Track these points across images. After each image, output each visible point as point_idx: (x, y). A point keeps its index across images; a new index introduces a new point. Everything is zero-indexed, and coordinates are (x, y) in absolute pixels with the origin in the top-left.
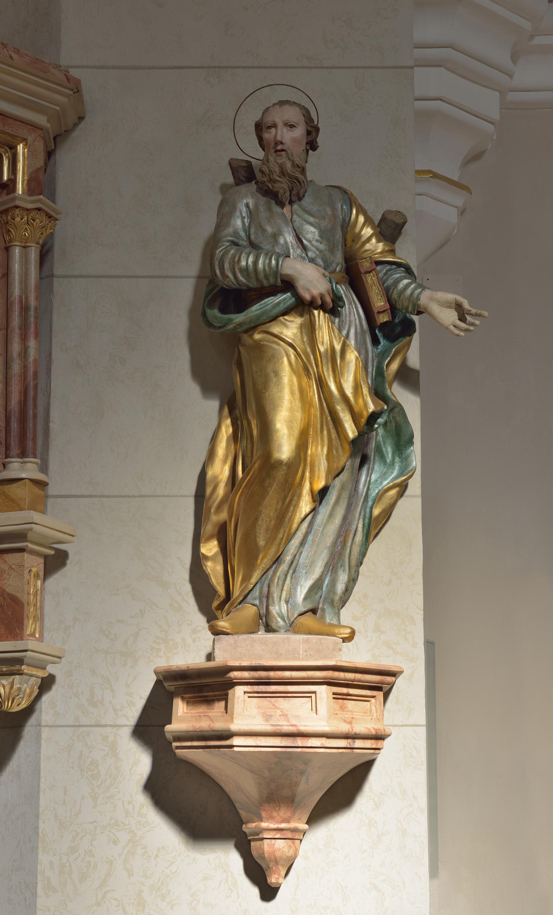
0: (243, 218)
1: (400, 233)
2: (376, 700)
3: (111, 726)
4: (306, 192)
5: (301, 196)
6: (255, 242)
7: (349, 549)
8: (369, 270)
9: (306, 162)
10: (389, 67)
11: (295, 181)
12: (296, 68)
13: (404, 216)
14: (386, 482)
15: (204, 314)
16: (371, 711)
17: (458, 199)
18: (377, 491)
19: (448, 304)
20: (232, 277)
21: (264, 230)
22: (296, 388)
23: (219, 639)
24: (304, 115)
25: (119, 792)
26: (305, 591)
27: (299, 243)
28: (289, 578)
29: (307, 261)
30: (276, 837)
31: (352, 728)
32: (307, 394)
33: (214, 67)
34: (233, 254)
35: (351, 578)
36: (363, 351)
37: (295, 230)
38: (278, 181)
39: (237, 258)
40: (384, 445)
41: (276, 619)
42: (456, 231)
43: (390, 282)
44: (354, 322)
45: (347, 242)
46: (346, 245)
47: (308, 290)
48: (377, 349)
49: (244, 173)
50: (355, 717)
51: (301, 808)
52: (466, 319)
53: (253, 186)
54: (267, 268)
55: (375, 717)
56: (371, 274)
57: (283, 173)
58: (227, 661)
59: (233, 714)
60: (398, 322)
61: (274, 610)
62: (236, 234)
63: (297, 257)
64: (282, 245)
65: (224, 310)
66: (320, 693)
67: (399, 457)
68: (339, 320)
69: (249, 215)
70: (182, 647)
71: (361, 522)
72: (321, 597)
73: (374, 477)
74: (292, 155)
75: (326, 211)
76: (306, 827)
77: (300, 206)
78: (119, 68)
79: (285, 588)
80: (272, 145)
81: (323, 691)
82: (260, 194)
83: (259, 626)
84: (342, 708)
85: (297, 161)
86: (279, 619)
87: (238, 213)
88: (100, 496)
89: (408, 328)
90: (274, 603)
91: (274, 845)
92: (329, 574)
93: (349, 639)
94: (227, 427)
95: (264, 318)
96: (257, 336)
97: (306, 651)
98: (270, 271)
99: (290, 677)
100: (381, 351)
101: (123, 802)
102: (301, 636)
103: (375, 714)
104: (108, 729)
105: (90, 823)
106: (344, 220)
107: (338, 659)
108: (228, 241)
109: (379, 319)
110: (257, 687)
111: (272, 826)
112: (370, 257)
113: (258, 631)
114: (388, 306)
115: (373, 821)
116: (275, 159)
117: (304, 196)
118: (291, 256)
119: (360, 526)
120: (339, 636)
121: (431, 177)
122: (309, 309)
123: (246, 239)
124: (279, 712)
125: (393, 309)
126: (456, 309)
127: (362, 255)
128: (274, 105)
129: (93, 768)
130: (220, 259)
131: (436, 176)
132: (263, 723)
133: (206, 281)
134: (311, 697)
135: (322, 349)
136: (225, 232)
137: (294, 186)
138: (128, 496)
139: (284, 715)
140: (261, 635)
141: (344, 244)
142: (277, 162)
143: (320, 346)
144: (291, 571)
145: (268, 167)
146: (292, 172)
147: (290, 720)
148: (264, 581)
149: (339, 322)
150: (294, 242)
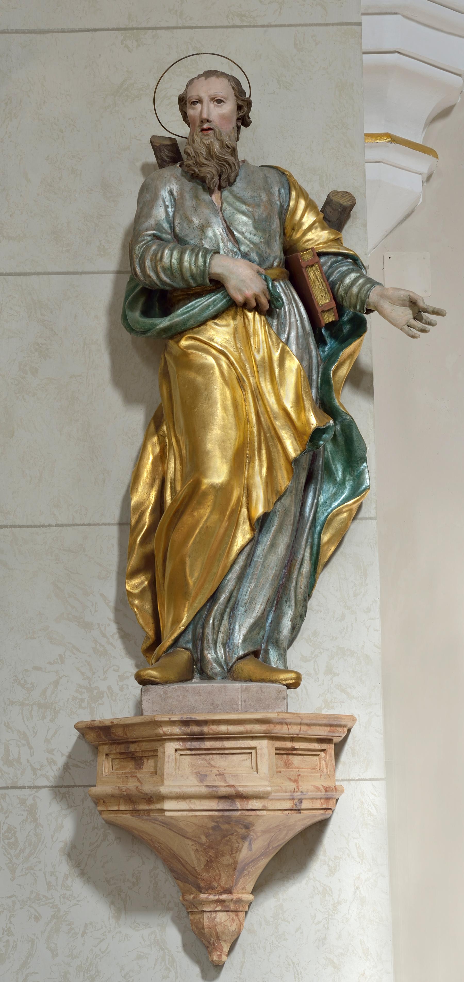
0: (166, 207)
1: (348, 216)
2: (326, 754)
3: (29, 787)
4: (237, 176)
5: (232, 181)
6: (180, 235)
7: (294, 582)
8: (311, 264)
9: (238, 139)
10: (333, 24)
11: (225, 164)
12: (227, 27)
13: (353, 197)
14: (336, 504)
15: (125, 317)
16: (320, 767)
17: (423, 164)
18: (326, 514)
19: (401, 302)
20: (153, 276)
21: (190, 222)
22: (229, 402)
23: (147, 690)
24: (233, 88)
25: (40, 862)
26: (244, 631)
27: (230, 235)
28: (226, 618)
29: (240, 257)
30: (217, 909)
31: (298, 787)
32: (242, 408)
33: (133, 29)
34: (155, 250)
35: (298, 614)
36: (306, 357)
37: (225, 221)
38: (204, 164)
39: (159, 255)
40: (333, 462)
41: (212, 665)
42: (421, 201)
43: (335, 276)
44: (294, 324)
45: (286, 231)
46: (284, 234)
47: (240, 290)
48: (324, 352)
49: (169, 153)
50: (302, 774)
51: (244, 876)
52: (422, 318)
53: (177, 169)
54: (193, 267)
55: (325, 773)
56: (314, 268)
57: (210, 155)
58: (154, 716)
59: (163, 775)
60: (347, 320)
61: (210, 655)
62: (158, 227)
63: (228, 252)
64: (211, 238)
65: (146, 313)
66: (261, 749)
67: (350, 474)
68: (278, 322)
69: (173, 203)
70: (108, 697)
71: (308, 550)
72: (263, 637)
73: (322, 499)
74: (221, 134)
75: (260, 197)
76: (251, 897)
77: (231, 192)
78: (23, 32)
79: (222, 629)
80: (198, 123)
81: (263, 745)
82: (186, 178)
83: (193, 672)
84: (286, 765)
85: (227, 141)
86: (215, 665)
87: (160, 202)
88: (11, 527)
89: (358, 327)
90: (209, 646)
91: (215, 918)
92: (273, 610)
93: (294, 685)
94: (154, 445)
95: (191, 322)
96: (184, 343)
97: (245, 701)
98: (197, 270)
99: (226, 732)
100: (328, 354)
101: (45, 873)
102: (240, 685)
103: (325, 770)
104: (26, 791)
105: (8, 897)
106: (282, 206)
107: (283, 708)
108: (150, 235)
109: (323, 319)
110: (189, 743)
111: (212, 897)
112: (312, 249)
113: (192, 678)
114: (334, 305)
115: (327, 888)
116: (201, 139)
117: (235, 181)
118: (222, 252)
119: (307, 554)
120: (283, 682)
121: (389, 141)
122: (243, 311)
123: (170, 231)
124: (215, 771)
125: (340, 308)
126: (410, 306)
127: (304, 246)
128: (199, 76)
129: (10, 835)
130: (141, 256)
131: (394, 140)
132: (198, 784)
133: (127, 278)
134: (251, 753)
135: (258, 357)
136: (146, 225)
137: (224, 170)
138: (44, 526)
139: (221, 775)
140: (196, 684)
141: (282, 234)
142: (203, 143)
143: (256, 354)
144: (228, 610)
145: (193, 148)
146: (221, 154)
147: (227, 779)
148: (198, 622)
149: (277, 325)
150: (224, 235)
